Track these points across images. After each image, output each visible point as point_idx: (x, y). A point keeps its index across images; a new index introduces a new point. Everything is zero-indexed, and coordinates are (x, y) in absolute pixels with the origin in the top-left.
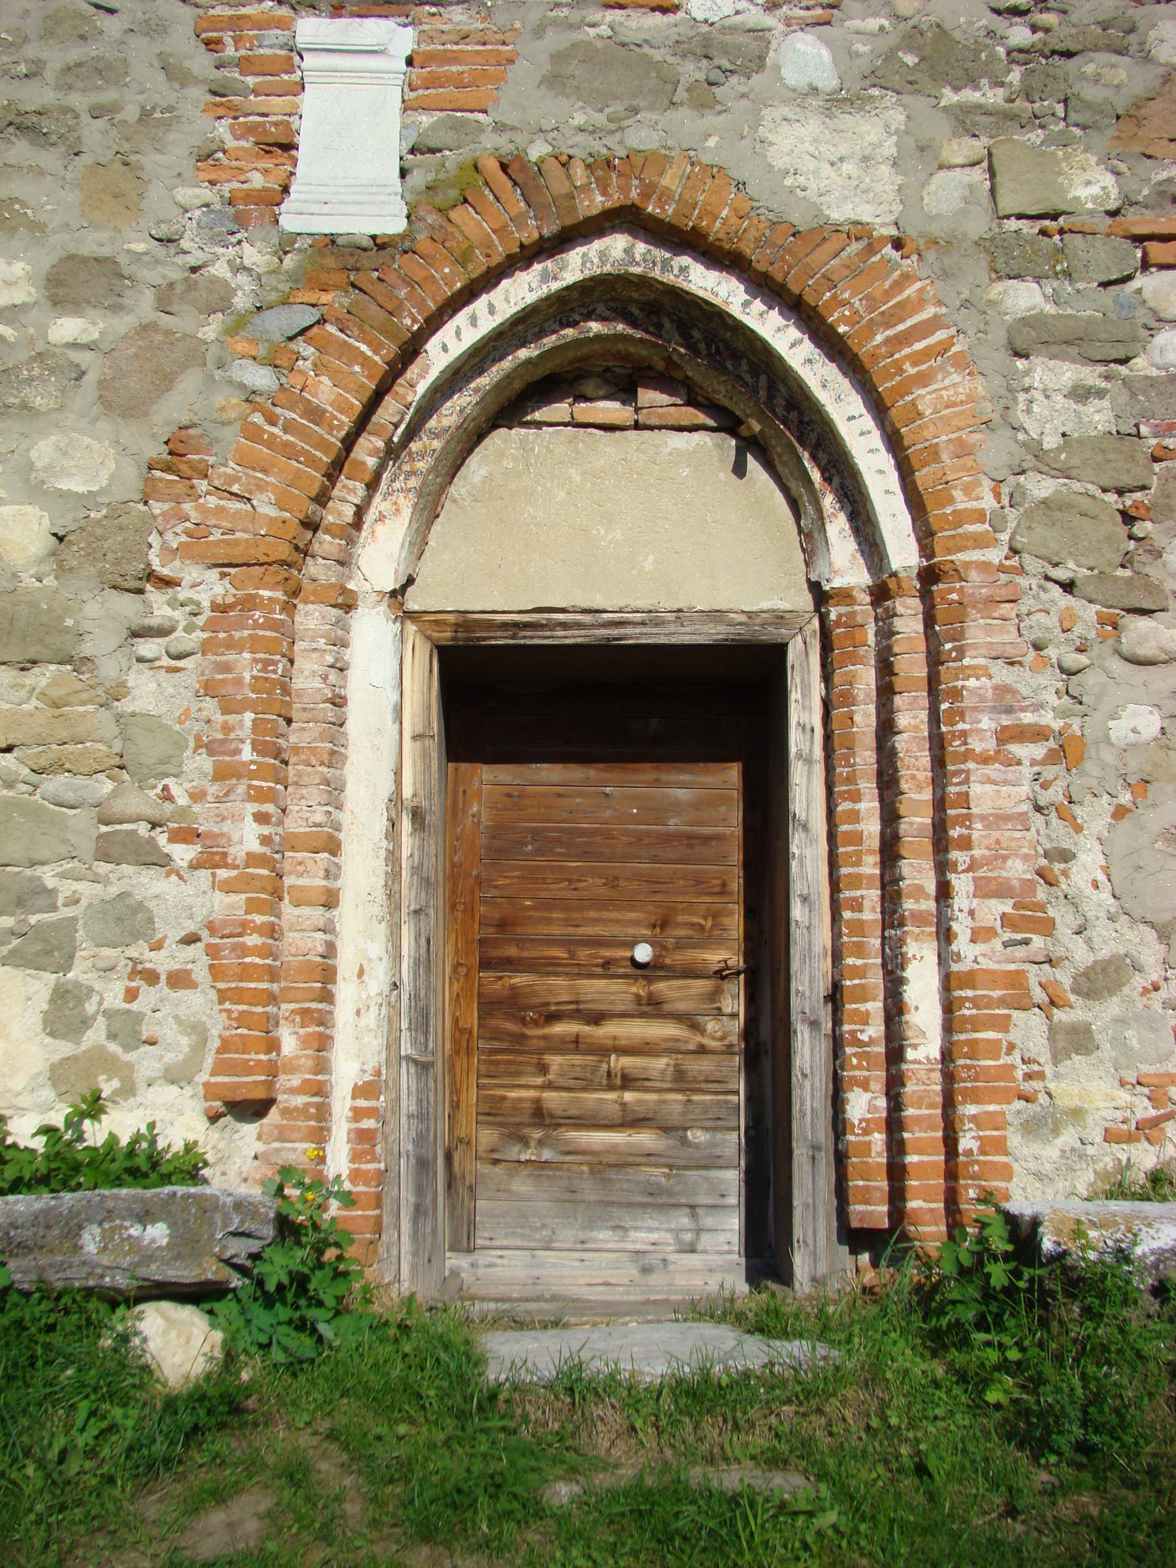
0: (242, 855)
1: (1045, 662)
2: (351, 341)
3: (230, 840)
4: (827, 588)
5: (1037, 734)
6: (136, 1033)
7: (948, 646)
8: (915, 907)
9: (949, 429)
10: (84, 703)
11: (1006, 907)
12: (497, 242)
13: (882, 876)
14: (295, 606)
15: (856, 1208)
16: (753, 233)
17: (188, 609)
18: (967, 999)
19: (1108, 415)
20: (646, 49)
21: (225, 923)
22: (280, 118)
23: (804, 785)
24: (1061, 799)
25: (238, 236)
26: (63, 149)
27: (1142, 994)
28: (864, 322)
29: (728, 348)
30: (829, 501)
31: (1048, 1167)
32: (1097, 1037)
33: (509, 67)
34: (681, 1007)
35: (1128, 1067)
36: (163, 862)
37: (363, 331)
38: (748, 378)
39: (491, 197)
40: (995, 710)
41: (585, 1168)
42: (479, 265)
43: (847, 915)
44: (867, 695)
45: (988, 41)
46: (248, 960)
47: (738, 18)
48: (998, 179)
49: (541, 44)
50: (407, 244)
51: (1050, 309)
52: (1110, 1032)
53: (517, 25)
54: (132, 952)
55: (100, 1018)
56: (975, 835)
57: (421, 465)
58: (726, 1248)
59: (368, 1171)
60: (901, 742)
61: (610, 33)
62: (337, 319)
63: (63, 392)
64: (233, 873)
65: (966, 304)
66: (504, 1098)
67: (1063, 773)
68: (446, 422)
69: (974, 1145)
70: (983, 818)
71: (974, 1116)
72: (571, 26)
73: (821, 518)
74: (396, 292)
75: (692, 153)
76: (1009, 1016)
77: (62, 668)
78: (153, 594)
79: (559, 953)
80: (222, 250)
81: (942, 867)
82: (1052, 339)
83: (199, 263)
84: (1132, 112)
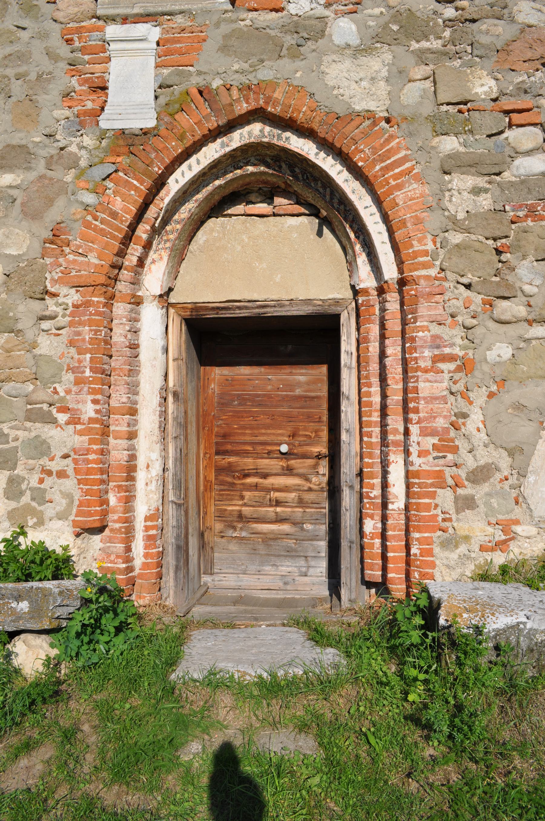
0: (87, 418)
1: (456, 323)
2: (130, 179)
3: (81, 412)
4: (357, 288)
5: (452, 358)
6: (44, 498)
7: (410, 316)
8: (394, 438)
9: (411, 211)
10: (19, 350)
11: (435, 440)
12: (197, 129)
13: (381, 421)
14: (112, 304)
15: (367, 572)
16: (318, 119)
17: (62, 307)
18: (416, 483)
19: (490, 201)
20: (268, 31)
21: (80, 449)
22: (100, 74)
23: (347, 379)
24: (462, 388)
25: (81, 132)
26: (3, 95)
27: (500, 482)
28: (370, 160)
29: (312, 176)
30: (358, 247)
31: (452, 563)
32: (478, 502)
33: (204, 43)
34: (301, 471)
35: (492, 516)
36: (54, 421)
37: (135, 175)
38: (321, 190)
39: (194, 107)
40: (431, 347)
41: (260, 540)
42: (189, 140)
43: (365, 439)
44: (375, 338)
45: (434, 16)
46: (90, 466)
47: (312, 12)
48: (437, 86)
49: (218, 31)
50: (156, 132)
51: (462, 149)
52: (484, 500)
53: (207, 22)
54: (41, 462)
55: (28, 491)
56: (421, 407)
57: (172, 237)
58: (320, 574)
59: (153, 553)
60: (388, 361)
61: (251, 24)
62: (123, 169)
63: (6, 208)
64: (83, 427)
65: (421, 149)
66: (226, 510)
67: (464, 376)
68: (183, 216)
69: (418, 552)
70: (425, 398)
71: (418, 538)
72: (232, 21)
73: (355, 255)
74: (150, 155)
75: (289, 80)
76: (436, 492)
77: (10, 334)
78: (49, 301)
79: (249, 448)
80: (74, 139)
81: (406, 421)
82: (462, 165)
83: (64, 146)
84: (505, 48)
